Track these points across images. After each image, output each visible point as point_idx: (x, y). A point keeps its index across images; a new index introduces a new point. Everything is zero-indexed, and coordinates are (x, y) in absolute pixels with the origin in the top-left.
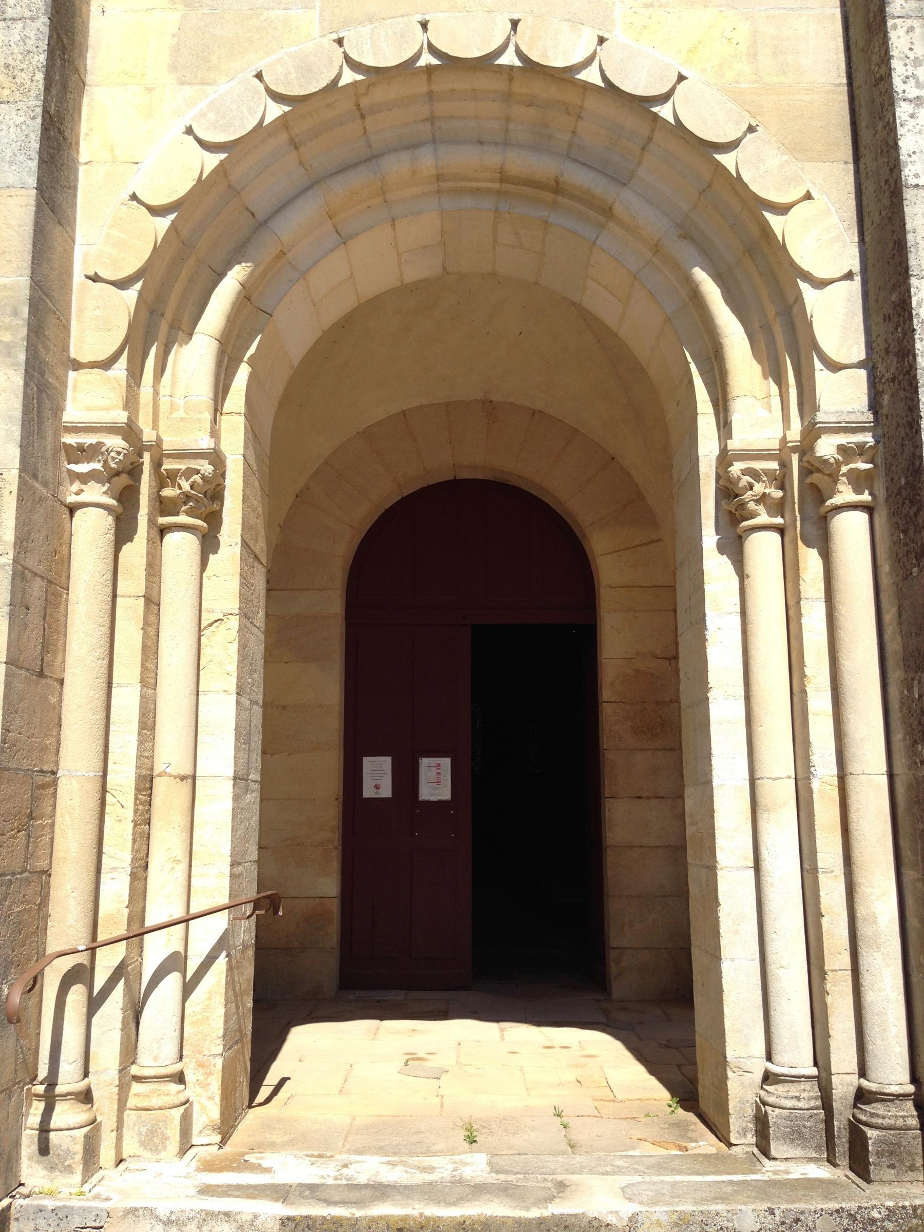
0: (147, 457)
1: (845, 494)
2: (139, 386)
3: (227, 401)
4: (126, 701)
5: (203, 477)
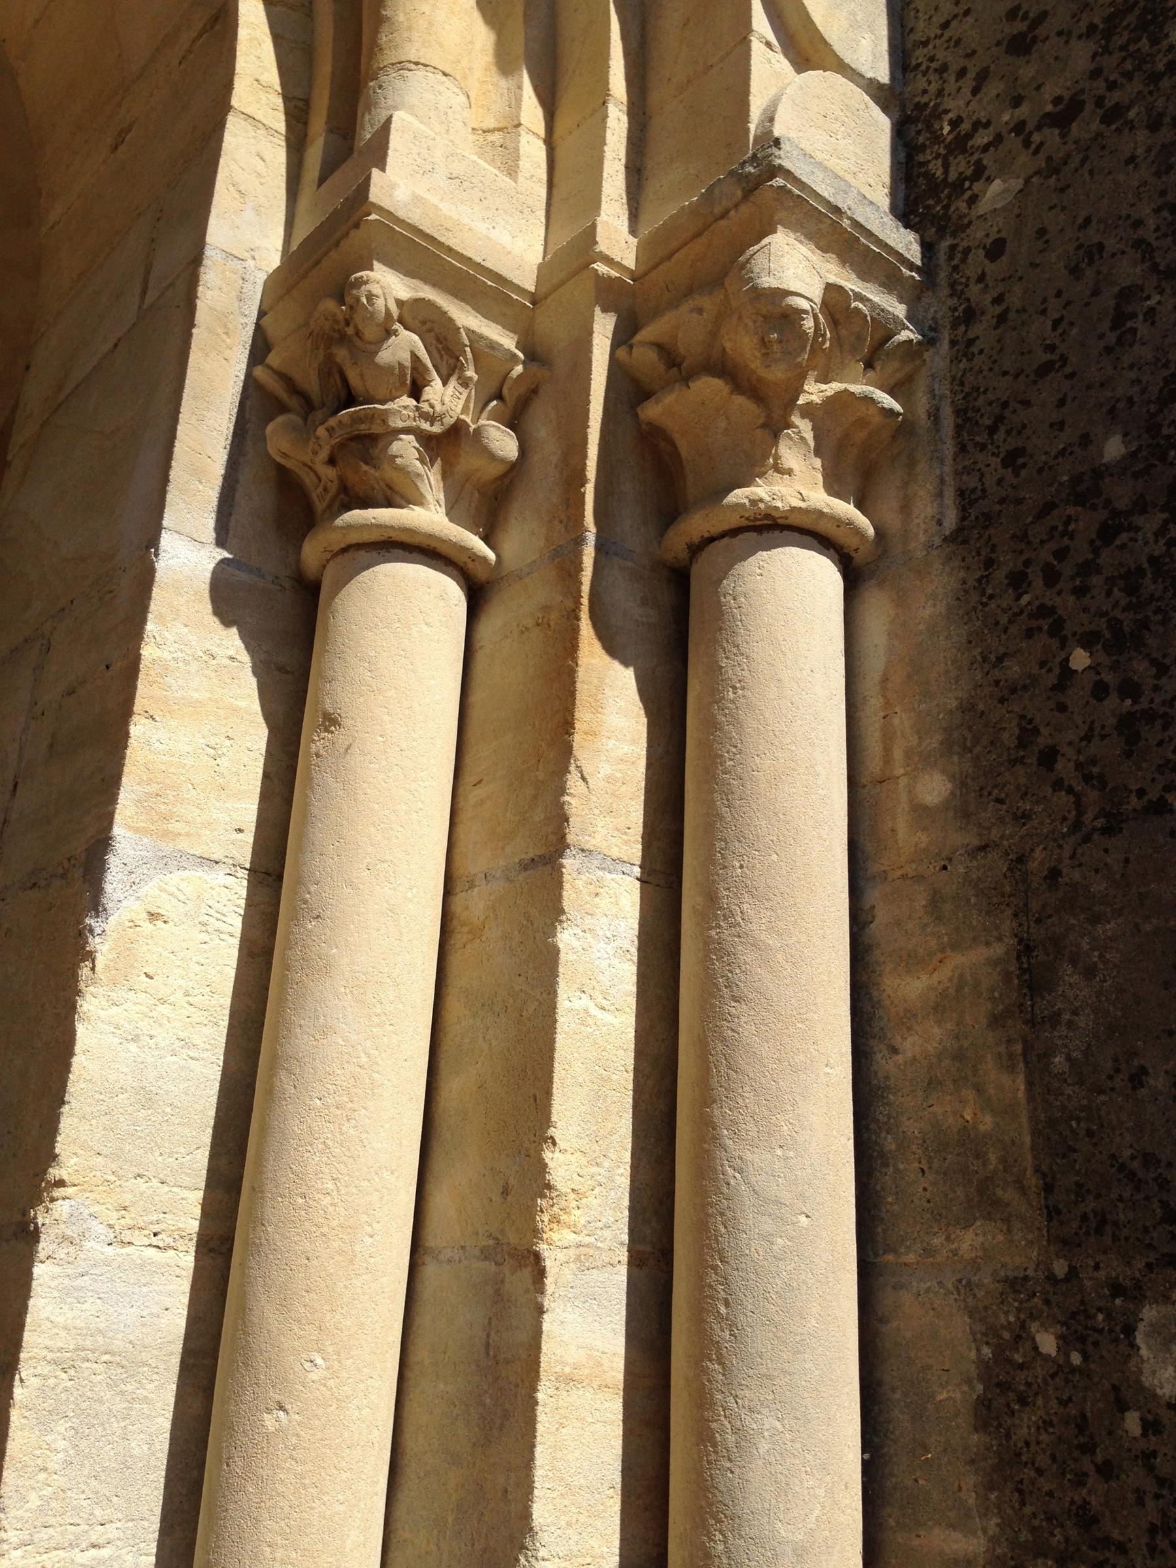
1: (796, 481)
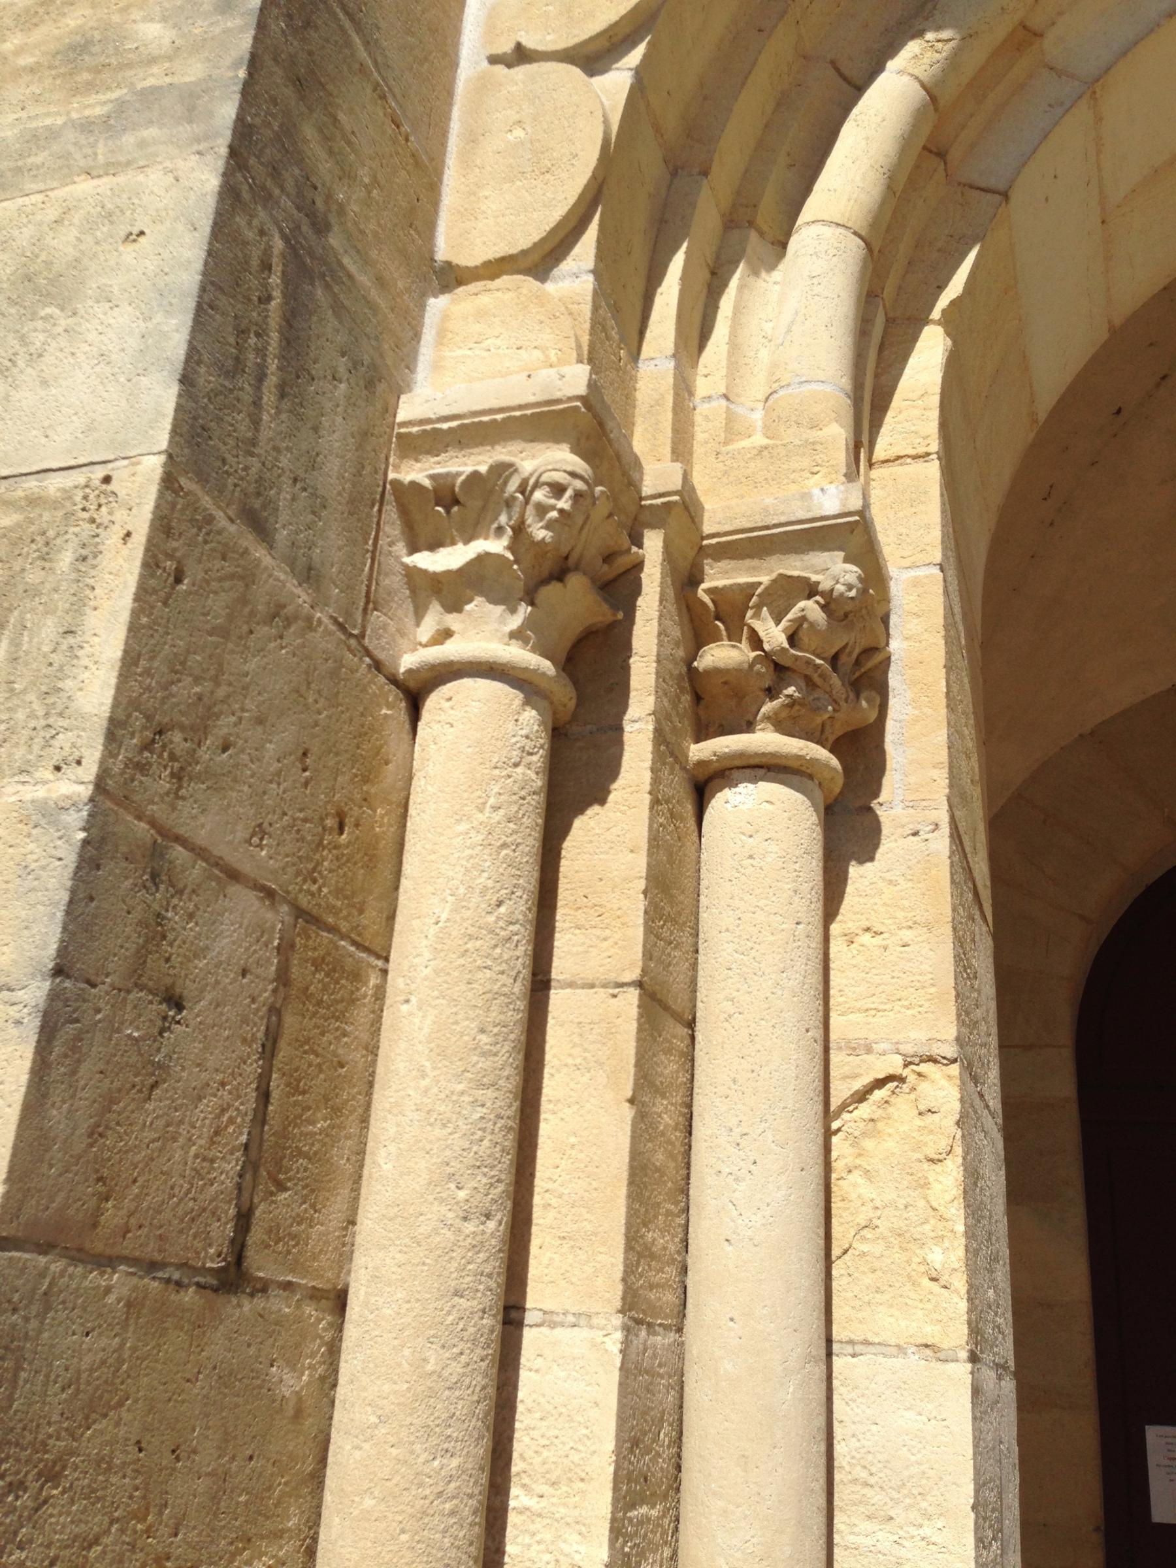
0: (653, 544)
2: (636, 355)
3: (884, 430)
4: (571, 1382)
5: (830, 603)
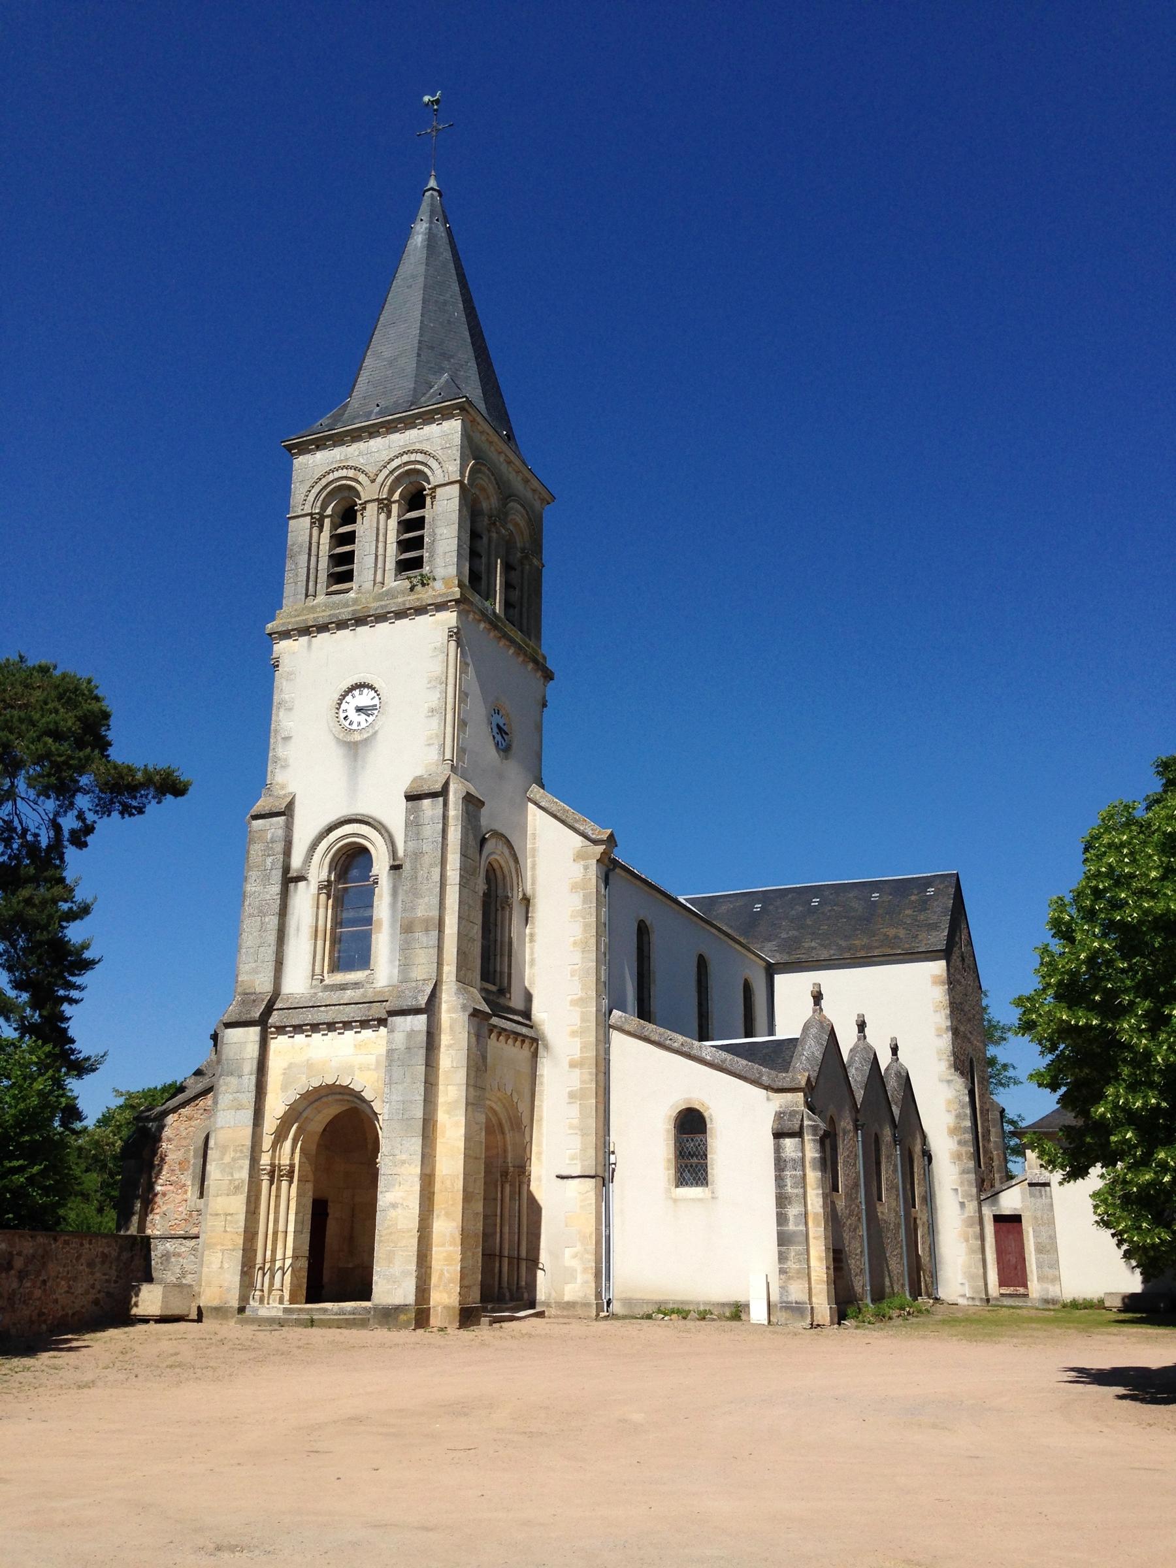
4: (269, 1247)
